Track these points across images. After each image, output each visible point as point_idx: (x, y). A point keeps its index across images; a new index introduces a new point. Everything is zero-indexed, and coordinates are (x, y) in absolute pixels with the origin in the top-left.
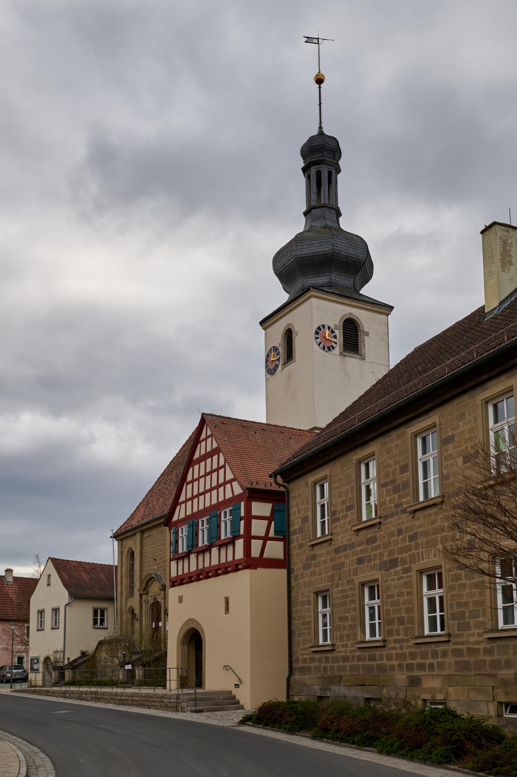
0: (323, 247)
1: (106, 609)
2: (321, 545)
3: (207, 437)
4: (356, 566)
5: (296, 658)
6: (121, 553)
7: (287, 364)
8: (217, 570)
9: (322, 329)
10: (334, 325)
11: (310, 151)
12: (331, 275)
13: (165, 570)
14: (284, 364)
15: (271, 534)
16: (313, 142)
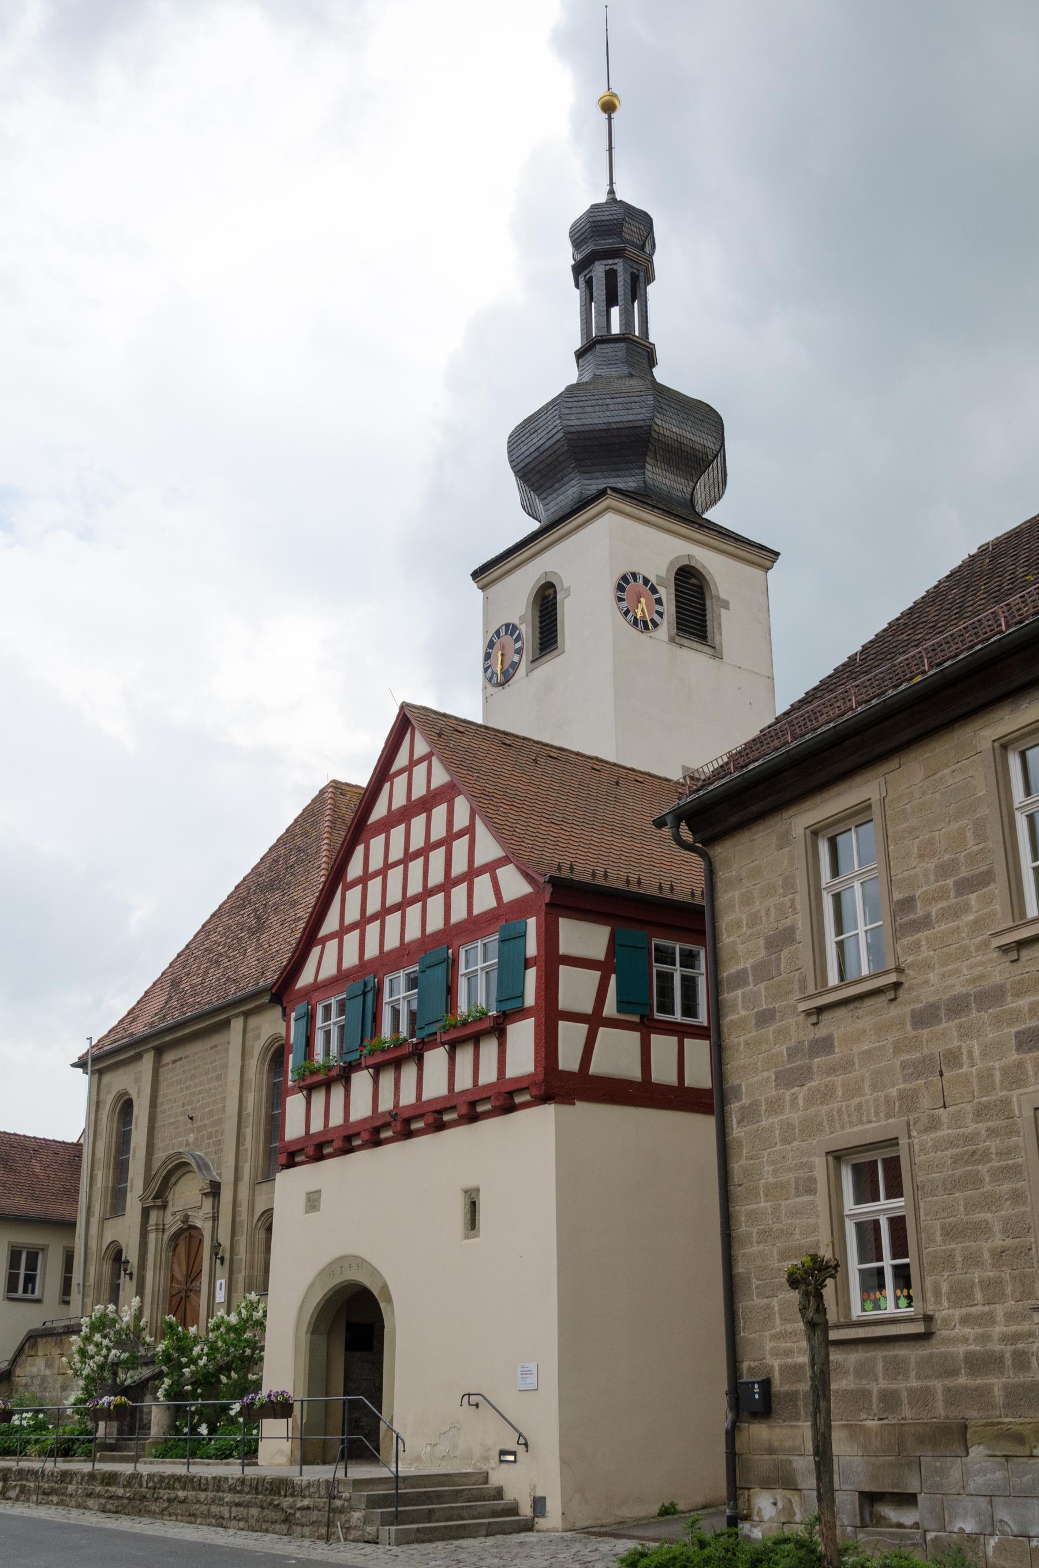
0: (631, 412)
1: (43, 1250)
2: (851, 1006)
3: (413, 763)
4: (1014, 1057)
5: (753, 1364)
6: (95, 1105)
7: (540, 660)
8: (440, 1112)
9: (631, 580)
10: (657, 576)
11: (594, 232)
12: (644, 473)
13: (219, 1143)
14: (533, 661)
15: (610, 1009)
16: (599, 214)
